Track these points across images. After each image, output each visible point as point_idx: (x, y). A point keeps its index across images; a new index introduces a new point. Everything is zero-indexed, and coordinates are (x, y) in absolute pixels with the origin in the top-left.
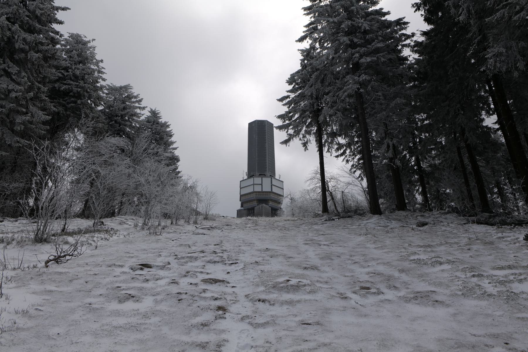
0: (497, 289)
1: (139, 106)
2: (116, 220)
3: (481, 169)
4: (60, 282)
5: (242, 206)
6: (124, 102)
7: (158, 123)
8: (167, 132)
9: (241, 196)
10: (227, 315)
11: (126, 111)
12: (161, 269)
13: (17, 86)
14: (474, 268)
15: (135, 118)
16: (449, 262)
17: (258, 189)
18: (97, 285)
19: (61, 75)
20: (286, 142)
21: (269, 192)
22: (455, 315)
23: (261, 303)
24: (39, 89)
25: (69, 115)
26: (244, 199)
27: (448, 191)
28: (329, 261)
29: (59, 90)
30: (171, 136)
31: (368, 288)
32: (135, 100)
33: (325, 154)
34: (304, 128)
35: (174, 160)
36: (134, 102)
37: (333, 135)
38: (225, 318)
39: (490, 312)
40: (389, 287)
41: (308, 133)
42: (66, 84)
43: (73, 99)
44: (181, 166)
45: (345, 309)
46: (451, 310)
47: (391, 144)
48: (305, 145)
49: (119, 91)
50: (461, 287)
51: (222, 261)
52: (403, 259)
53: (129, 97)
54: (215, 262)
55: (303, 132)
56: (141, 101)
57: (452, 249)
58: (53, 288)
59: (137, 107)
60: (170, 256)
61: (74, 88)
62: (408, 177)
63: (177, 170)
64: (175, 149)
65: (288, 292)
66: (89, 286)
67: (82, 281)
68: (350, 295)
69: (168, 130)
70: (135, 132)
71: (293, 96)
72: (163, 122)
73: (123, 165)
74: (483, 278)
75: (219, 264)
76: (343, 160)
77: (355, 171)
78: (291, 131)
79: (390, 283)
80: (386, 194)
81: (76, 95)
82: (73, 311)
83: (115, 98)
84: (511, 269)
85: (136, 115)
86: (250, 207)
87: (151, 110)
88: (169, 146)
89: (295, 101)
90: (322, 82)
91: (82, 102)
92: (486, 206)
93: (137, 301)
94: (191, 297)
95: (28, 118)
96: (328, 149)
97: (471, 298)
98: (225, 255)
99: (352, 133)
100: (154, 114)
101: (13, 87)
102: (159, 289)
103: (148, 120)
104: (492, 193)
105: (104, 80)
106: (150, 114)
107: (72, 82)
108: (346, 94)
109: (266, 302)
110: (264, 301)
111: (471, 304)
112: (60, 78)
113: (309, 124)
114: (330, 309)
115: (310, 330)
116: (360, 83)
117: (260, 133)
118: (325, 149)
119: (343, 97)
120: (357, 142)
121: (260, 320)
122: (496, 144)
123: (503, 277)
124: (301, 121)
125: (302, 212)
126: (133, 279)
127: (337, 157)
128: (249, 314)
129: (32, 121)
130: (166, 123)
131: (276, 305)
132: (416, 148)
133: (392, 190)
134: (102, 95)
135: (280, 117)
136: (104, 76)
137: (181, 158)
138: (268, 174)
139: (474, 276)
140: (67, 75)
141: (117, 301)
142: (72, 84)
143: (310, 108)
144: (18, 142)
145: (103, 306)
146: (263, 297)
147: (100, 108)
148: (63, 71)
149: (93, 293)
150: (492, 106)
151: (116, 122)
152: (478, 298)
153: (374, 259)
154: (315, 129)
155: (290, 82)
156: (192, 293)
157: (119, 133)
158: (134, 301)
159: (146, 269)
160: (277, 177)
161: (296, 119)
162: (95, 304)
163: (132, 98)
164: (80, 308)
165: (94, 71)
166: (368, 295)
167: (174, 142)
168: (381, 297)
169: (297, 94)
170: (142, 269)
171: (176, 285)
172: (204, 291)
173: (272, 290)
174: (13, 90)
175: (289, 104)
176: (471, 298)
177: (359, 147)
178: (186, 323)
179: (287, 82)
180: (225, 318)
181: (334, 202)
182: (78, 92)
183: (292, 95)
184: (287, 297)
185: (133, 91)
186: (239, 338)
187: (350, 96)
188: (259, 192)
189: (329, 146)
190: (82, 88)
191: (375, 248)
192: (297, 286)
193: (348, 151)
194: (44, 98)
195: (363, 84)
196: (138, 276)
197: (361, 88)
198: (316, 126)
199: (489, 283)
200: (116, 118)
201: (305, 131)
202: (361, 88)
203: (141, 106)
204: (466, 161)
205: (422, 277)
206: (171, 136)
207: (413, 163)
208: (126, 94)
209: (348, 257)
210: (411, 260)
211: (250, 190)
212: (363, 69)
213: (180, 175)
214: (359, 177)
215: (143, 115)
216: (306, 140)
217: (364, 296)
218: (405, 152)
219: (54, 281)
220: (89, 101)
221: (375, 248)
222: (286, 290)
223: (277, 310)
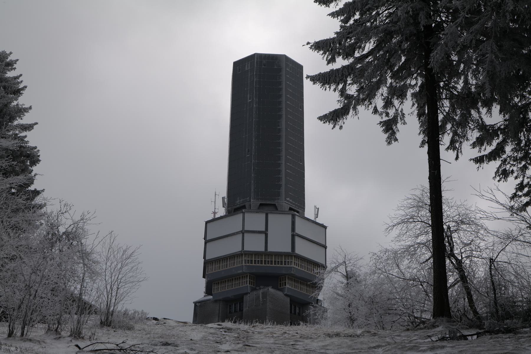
5: (209, 291)
8: (7, 80)
9: (207, 263)
17: (255, 244)
20: (334, 117)
26: (215, 271)
33: (442, 149)
37: (467, 101)
48: (390, 127)
63: (32, 188)
64: (28, 127)
69: (10, 74)
88: (12, 119)
113: (401, 68)
118: (446, 139)
124: (384, 59)
125: (373, 309)
127: (479, 160)
138: (284, 203)
160: (309, 213)
167: (26, 110)
188: (257, 254)
189: (455, 133)
193: (508, 149)
198: (420, 75)
201: (391, 87)
211: (233, 246)
213: (38, 200)
216: (392, 112)
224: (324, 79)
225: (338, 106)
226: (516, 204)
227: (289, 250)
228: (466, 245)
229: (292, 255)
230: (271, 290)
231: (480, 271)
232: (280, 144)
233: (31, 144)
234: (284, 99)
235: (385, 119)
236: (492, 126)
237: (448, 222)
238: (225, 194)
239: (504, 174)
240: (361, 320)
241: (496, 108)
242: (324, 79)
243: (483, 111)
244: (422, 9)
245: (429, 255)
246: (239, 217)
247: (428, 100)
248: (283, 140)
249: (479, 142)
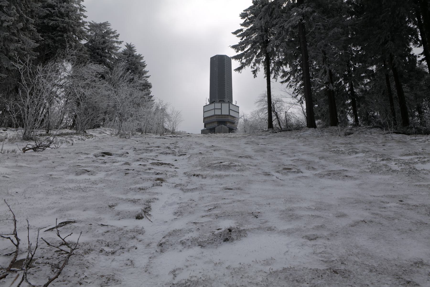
0: (400, 167)
1: (117, 40)
2: (97, 130)
3: (405, 94)
4: (31, 161)
5: (205, 127)
6: (103, 37)
7: (133, 56)
8: (141, 63)
9: (204, 118)
10: (164, 184)
11: (106, 45)
12: (120, 156)
13: (8, 17)
14: (384, 155)
15: (113, 51)
16: (363, 152)
17: (218, 112)
18: (62, 164)
19: (48, 12)
20: (239, 69)
21: (227, 115)
22: (360, 184)
23: (195, 177)
24: (27, 20)
25: (58, 46)
26: (207, 121)
27: (376, 114)
28: (262, 153)
29: (48, 26)
30: (144, 66)
31: (290, 169)
32: (113, 35)
33: (271, 78)
34: (255, 58)
35: (147, 86)
36: (112, 37)
37: (279, 64)
38: (162, 186)
39: (392, 182)
40: (308, 168)
41: (258, 61)
42: (53, 20)
43: (60, 33)
44: (153, 91)
45: (265, 181)
46: (358, 182)
47: (327, 69)
48: (254, 72)
49: (99, 27)
50: (370, 167)
51: (173, 153)
52: (324, 150)
53: (108, 33)
54: (167, 153)
55: (254, 61)
56: (117, 36)
57: (369, 145)
58: (23, 165)
59: (115, 42)
60: (130, 149)
61: (60, 24)
62: (342, 100)
63: (150, 95)
64: (148, 77)
65: (220, 170)
66: (55, 164)
67: (50, 161)
68: (273, 173)
69: (142, 61)
70: (114, 63)
71: (245, 29)
72: (137, 55)
73: (103, 88)
74: (391, 161)
75: (170, 155)
76: (287, 86)
77: (297, 95)
78: (244, 61)
79: (310, 165)
80: (323, 115)
81: (62, 29)
82: (35, 179)
83: (96, 34)
84: (418, 155)
85: (114, 48)
86: (211, 128)
87: (127, 44)
88: (143, 74)
89: (247, 34)
90: (271, 15)
91: (67, 36)
92: (406, 123)
93: (92, 174)
94: (137, 172)
95: (19, 45)
96: (274, 76)
97: (377, 174)
98: (177, 150)
99: (296, 62)
100: (130, 48)
101: (5, 18)
102: (113, 168)
103: (125, 53)
104: (413, 116)
105: (85, 17)
106: (126, 48)
107: (58, 18)
108: (290, 24)
109: (200, 176)
110: (198, 176)
111: (376, 178)
112: (48, 14)
113: (259, 54)
114: (252, 181)
115: (231, 192)
116: (303, 15)
117: (220, 69)
118: (272, 76)
119: (288, 26)
120: (300, 70)
121: (190, 187)
122: (420, 73)
123: (408, 160)
124: (253, 51)
125: (252, 129)
126: (93, 161)
127: (282, 82)
128: (182, 183)
129: (24, 48)
130: (139, 55)
131: (208, 178)
132: (350, 76)
133: (327, 110)
134: (84, 29)
135: (234, 47)
136: (85, 14)
137: (153, 85)
138: (227, 100)
139: (383, 160)
140: (54, 13)
141: (75, 174)
142: (58, 20)
143: (260, 40)
144: (14, 66)
145: (62, 177)
146: (198, 173)
147: (84, 42)
148: (50, 9)
149: (57, 169)
150: (420, 38)
151: (98, 54)
152: (384, 173)
153: (300, 151)
154: (264, 58)
155: (243, 16)
156: (138, 170)
157: (101, 62)
158: (89, 175)
159: (107, 157)
160: (234, 103)
161: (248, 50)
162: (55, 175)
163: (110, 33)
164: (42, 178)
165: (76, 9)
166: (289, 173)
167: (147, 72)
168: (300, 175)
169: (249, 27)
170: (103, 156)
171: (128, 165)
172: (150, 169)
173: (207, 169)
174: (5, 20)
175: (243, 35)
176: (377, 174)
177: (300, 75)
178: (126, 188)
179: (241, 16)
180: (162, 186)
181: (278, 120)
182: (64, 27)
183: (245, 29)
184: (218, 173)
185: (111, 27)
186: (169, 198)
187: (294, 27)
188: (219, 115)
189: (275, 73)
190: (68, 23)
191: (304, 145)
192: (228, 166)
193: (292, 78)
194: (32, 28)
195: (305, 16)
196: (98, 160)
197: (303, 19)
198: (265, 55)
199: (396, 164)
200: (97, 51)
201: (256, 60)
202: (303, 19)
203: (119, 40)
204: (393, 85)
205: (338, 162)
206: (144, 66)
207: (347, 89)
208: (105, 31)
209: (279, 151)
210: (331, 151)
211: (212, 113)
212: (306, 3)
213: (152, 99)
214: (300, 100)
215: (120, 48)
216: (255, 68)
217: (286, 174)
218: (341, 80)
219: (27, 161)
220: (74, 36)
221: (304, 145)
222: (219, 168)
223: (207, 181)
224: (236, 58)
225: (240, 66)
226: (294, 95)
227: (228, 114)
228: (278, 108)
229: (229, 115)
230: (223, 126)
231: (282, 116)
232: (225, 83)
233: (149, 82)
234: (226, 69)
235: (253, 70)
236: (287, 72)
237: (273, 101)
238: (209, 98)
239: (291, 86)
240: (248, 131)
241: (288, 65)
242: (236, 58)
243: (284, 67)
244: (265, 34)
245: (267, 111)
246: (213, 104)
247: (267, 64)
248: (226, 81)
249: (283, 76)
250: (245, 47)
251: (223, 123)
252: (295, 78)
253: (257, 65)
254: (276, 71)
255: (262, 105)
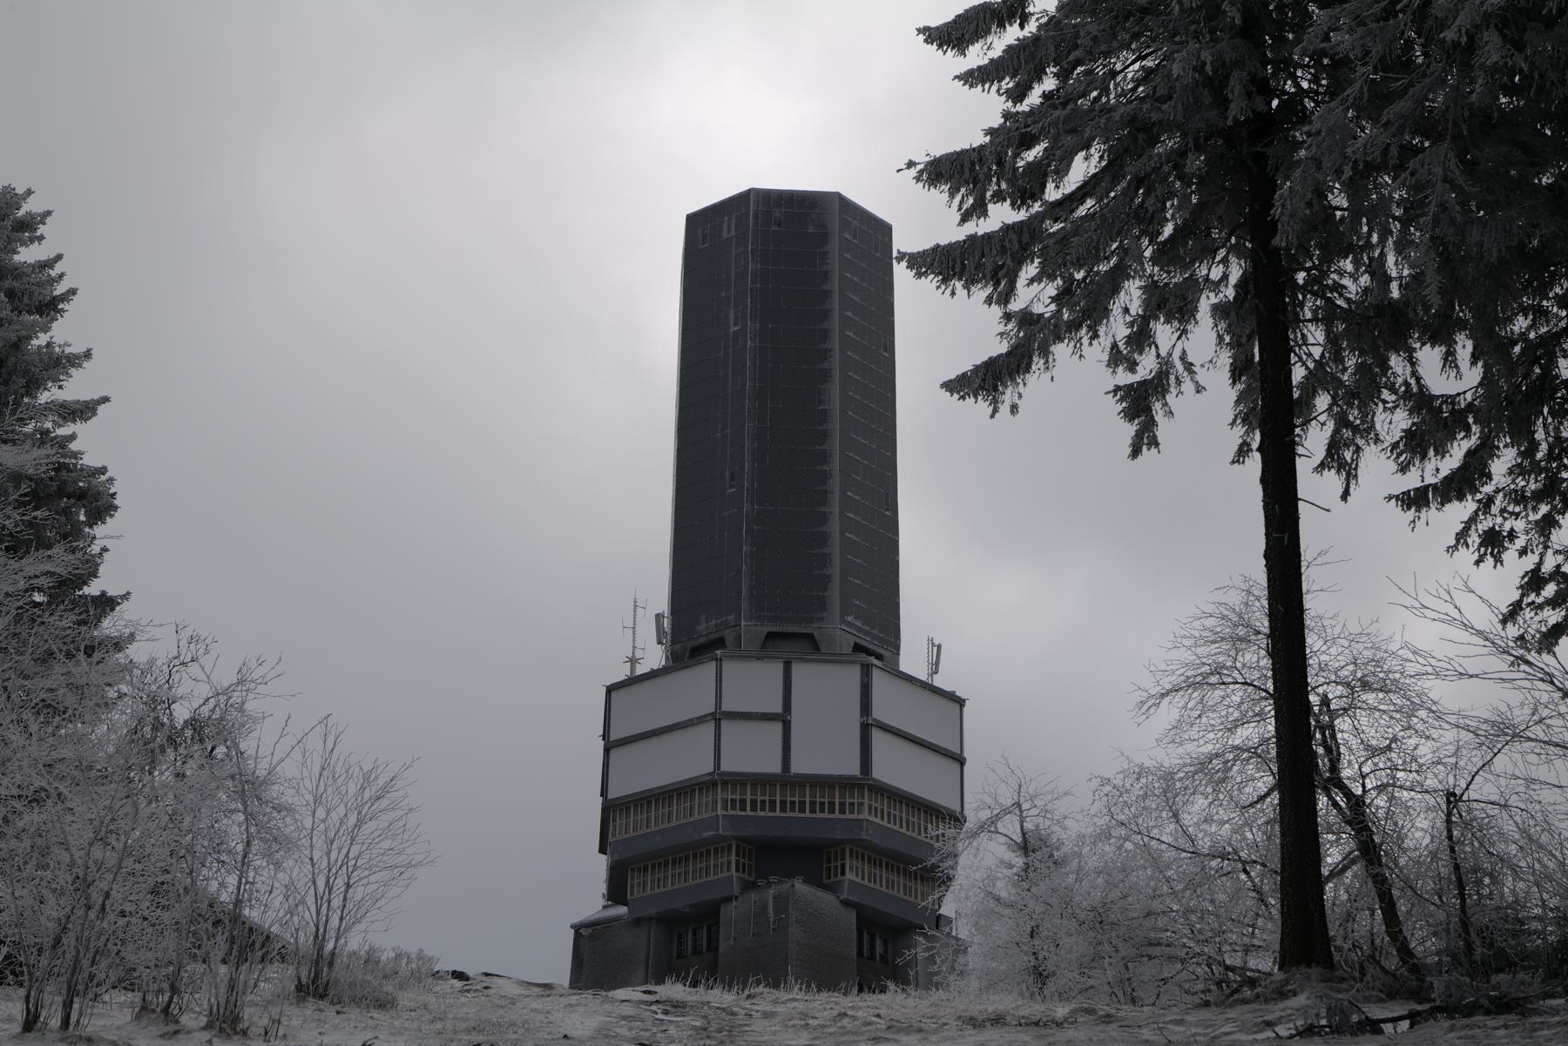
5: (616, 892)
8: (18, 272)
9: (611, 810)
17: (752, 752)
26: (637, 833)
30: (50, 308)
33: (1304, 468)
37: (1382, 327)
41: (1174, 304)
48: (1140, 403)
55: (1132, 295)
63: (93, 589)
64: (83, 411)
69: (27, 255)
76: (1462, 536)
88: (33, 385)
96: (1334, 447)
118: (1314, 440)
124: (1125, 206)
127: (1415, 500)
137: (123, 493)
138: (840, 630)
154: (1235, 274)
160: (912, 660)
167: (75, 361)
188: (760, 781)
189: (1342, 421)
193: (1502, 464)
198: (1237, 250)
211: (687, 759)
213: (110, 626)
216: (1147, 365)
225: (1003, 348)
227: (854, 769)
228: (1374, 752)
229: (863, 784)
230: (800, 887)
231: (1420, 830)
234: (835, 322)
235: (1124, 378)
236: (1451, 399)
237: (1322, 686)
238: (662, 603)
239: (1494, 542)
243: (1429, 357)
245: (1265, 781)
246: (706, 671)
247: (1261, 326)
248: (835, 445)
249: (1415, 445)
250: (1058, 163)
251: (810, 857)
252: (1535, 468)
253: (1164, 333)
254: (1352, 395)
255: (1213, 718)
